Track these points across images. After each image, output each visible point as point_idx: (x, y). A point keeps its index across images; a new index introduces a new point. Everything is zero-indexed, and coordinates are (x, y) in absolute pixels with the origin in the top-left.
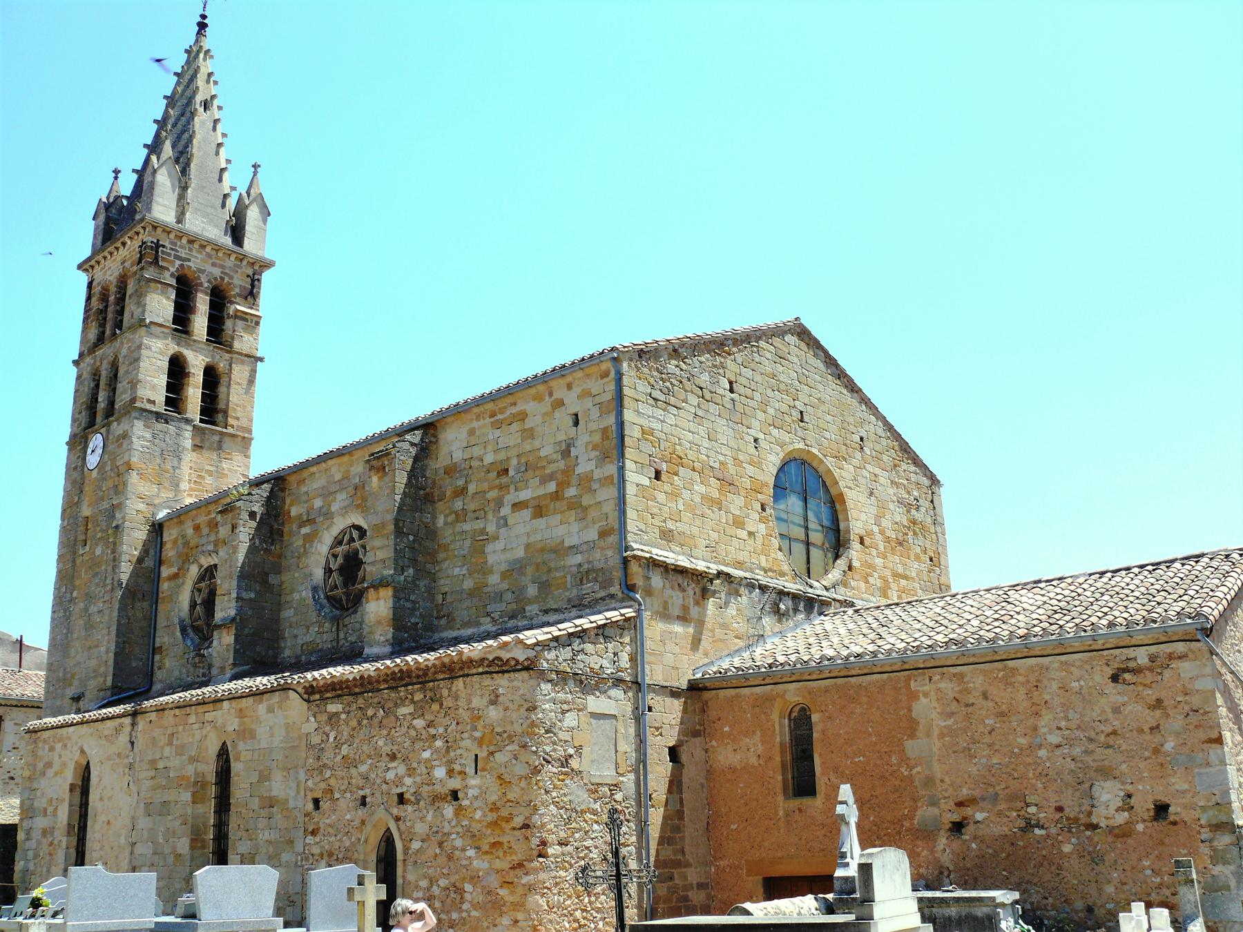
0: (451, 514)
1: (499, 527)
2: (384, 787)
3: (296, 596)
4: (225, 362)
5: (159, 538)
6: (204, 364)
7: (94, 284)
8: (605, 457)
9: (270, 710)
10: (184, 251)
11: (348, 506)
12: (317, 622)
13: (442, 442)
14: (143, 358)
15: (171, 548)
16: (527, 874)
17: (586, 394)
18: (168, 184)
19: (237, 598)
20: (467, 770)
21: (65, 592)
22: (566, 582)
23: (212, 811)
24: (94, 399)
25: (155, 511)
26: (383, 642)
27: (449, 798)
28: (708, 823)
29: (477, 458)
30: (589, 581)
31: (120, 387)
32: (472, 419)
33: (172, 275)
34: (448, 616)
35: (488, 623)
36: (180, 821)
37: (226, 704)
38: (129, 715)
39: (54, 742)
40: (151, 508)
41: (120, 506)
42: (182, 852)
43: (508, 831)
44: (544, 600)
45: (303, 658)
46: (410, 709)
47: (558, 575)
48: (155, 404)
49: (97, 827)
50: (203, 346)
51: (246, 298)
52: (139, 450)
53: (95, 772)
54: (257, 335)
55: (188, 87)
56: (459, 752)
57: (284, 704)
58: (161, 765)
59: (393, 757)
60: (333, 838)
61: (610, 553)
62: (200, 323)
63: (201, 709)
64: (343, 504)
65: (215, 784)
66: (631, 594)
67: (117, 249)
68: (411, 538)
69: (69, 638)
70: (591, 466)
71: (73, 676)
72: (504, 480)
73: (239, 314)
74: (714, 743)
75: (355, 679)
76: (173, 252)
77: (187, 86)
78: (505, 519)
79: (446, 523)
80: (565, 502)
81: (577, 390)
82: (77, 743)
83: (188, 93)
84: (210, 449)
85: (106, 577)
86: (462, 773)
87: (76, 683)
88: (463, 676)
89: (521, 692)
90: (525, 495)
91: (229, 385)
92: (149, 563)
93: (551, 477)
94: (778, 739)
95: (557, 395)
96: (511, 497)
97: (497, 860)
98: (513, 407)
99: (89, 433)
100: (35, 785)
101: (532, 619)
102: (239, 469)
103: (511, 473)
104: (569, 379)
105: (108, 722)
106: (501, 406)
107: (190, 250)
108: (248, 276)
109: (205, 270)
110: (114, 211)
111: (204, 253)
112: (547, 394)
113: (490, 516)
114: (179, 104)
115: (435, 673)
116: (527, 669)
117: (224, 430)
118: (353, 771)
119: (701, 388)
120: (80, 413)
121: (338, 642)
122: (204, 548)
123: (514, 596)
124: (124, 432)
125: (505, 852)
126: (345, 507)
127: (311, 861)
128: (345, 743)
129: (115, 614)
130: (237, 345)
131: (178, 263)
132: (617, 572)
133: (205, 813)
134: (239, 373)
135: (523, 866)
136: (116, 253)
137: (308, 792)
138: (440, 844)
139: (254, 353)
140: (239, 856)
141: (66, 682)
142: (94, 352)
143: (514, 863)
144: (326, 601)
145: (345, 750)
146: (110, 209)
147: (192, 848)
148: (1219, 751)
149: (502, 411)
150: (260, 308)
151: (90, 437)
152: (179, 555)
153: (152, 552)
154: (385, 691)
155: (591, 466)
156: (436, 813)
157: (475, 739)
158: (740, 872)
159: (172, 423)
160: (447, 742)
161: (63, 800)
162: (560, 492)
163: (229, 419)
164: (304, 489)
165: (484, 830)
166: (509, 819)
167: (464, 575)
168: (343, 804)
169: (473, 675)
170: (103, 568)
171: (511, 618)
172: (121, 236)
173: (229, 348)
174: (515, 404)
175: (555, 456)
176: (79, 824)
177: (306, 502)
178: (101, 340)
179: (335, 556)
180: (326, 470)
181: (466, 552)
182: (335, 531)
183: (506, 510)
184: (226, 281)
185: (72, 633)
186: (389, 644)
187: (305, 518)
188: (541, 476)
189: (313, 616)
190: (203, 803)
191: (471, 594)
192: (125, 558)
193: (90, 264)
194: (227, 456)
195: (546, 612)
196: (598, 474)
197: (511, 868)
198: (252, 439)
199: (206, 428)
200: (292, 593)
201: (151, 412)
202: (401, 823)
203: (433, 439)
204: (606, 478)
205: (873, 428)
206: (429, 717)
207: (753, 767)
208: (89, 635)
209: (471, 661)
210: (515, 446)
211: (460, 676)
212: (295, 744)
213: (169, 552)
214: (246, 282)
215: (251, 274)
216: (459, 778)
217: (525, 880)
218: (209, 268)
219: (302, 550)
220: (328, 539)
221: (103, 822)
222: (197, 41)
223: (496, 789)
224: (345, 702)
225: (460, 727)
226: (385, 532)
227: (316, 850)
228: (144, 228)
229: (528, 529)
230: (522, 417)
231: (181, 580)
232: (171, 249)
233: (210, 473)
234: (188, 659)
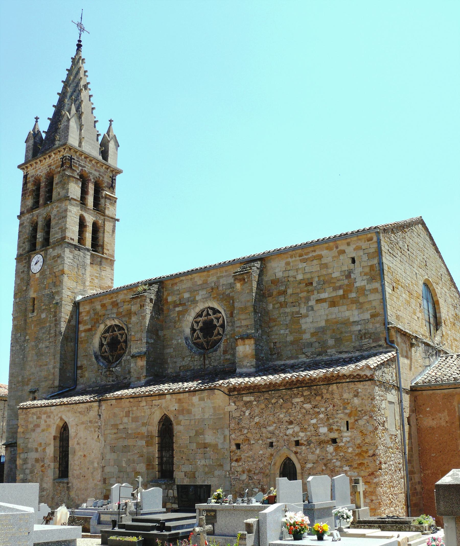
0: (277, 303)
1: (308, 310)
2: (285, 437)
3: (174, 342)
4: (102, 221)
5: (78, 310)
6: (93, 221)
7: (28, 176)
8: (372, 279)
9: (201, 399)
10: (83, 162)
11: (207, 297)
12: (189, 355)
13: (268, 268)
14: (68, 217)
15: (86, 316)
16: (375, 478)
17: (358, 248)
18: (75, 126)
19: (146, 342)
20: (342, 428)
21: (20, 336)
22: (352, 338)
23: (157, 451)
24: (34, 237)
25: (75, 296)
26: (249, 366)
27: (330, 442)
28: (419, 454)
29: (292, 276)
30: (365, 338)
31: (52, 231)
32: (288, 257)
33: (78, 174)
34: (278, 353)
35: (304, 358)
36: (138, 456)
37: (168, 397)
38: (97, 401)
39: (40, 414)
40: (74, 294)
41: (58, 293)
42: (140, 471)
43: (366, 458)
44: (339, 347)
45: (181, 374)
46: (302, 399)
47: (347, 335)
48: (74, 241)
49: (76, 458)
50: (91, 212)
51: (110, 188)
52: (67, 264)
53: (72, 430)
54: (116, 208)
55: (76, 77)
56: (336, 420)
57: (211, 397)
58: (121, 427)
59: (291, 423)
60: (251, 463)
61: (378, 325)
63: (149, 399)
64: (203, 296)
65: (158, 437)
66: (393, 345)
67: (45, 159)
68: (260, 315)
69: (25, 360)
70: (364, 283)
71: (29, 380)
72: (310, 288)
73: (108, 196)
74: (421, 416)
75: (266, 384)
76: (78, 163)
77: (75, 77)
78: (312, 307)
79: (274, 308)
80: (349, 300)
81: (353, 246)
82: (57, 415)
83: (76, 80)
84: (96, 264)
85: (50, 329)
86: (339, 430)
87: (31, 383)
88: (336, 383)
89: (369, 391)
90: (324, 295)
91: (104, 232)
92: (73, 323)
93: (340, 288)
94: (457, 414)
95: (341, 248)
96: (315, 296)
97: (362, 471)
98: (313, 252)
99: (32, 254)
100: (27, 436)
101: (331, 356)
102: (109, 276)
103: (315, 284)
104: (349, 240)
105: (81, 405)
106: (306, 251)
107: (85, 162)
108: (110, 177)
109: (92, 173)
110: (37, 139)
111: (91, 164)
112: (335, 247)
113: (302, 305)
114: (72, 85)
115: (319, 381)
116: (370, 380)
117: (103, 256)
118: (264, 430)
119: (401, 248)
120: (24, 243)
121: (205, 366)
122: (109, 316)
123: (319, 345)
124: (58, 254)
125: (366, 468)
126: (206, 298)
127: (236, 475)
128: (256, 416)
129: (59, 348)
130: (107, 212)
131: (80, 168)
132: (383, 334)
133: (153, 451)
134: (108, 226)
136: (44, 161)
137: (232, 441)
138: (325, 465)
139: (114, 217)
140: (184, 473)
141: (25, 382)
142: (32, 212)
143: (370, 472)
144: (193, 345)
145: (257, 419)
146: (36, 138)
147: (147, 469)
149: (307, 254)
150: (116, 194)
151: (32, 256)
152: (92, 319)
153: (74, 317)
154: (284, 390)
155: (364, 283)
156: (322, 450)
157: (346, 414)
158: (438, 476)
159: (81, 251)
160: (327, 415)
161: (50, 444)
162: (346, 295)
163: (105, 250)
164: (176, 288)
165: (354, 457)
166: (366, 452)
167: (287, 334)
168: (257, 447)
169: (344, 383)
170: (48, 324)
172: (50, 152)
173: (104, 214)
174: (315, 251)
175: (341, 277)
176: (59, 456)
177: (178, 294)
178: (36, 205)
180: (191, 279)
181: (287, 323)
182: (198, 310)
183: (312, 303)
184: (101, 179)
185: (27, 358)
186: (254, 367)
187: (178, 303)
188: (333, 287)
189: (187, 352)
190: (151, 446)
191: (292, 343)
192: (63, 320)
193: (26, 165)
194: (104, 269)
195: (341, 353)
196: (368, 287)
197: (368, 475)
198: (115, 261)
199: (95, 254)
200: (172, 340)
201: (72, 244)
202: (298, 455)
203: (264, 266)
204: (373, 289)
205: (443, 270)
206: (314, 403)
207: (444, 427)
208: (40, 359)
209: (345, 375)
210: (316, 272)
211: (334, 383)
212: (221, 417)
213: (84, 317)
214: (110, 180)
215: (112, 176)
217: (375, 480)
218: (93, 172)
219: (177, 319)
220: (193, 314)
221: (81, 455)
222: (77, 54)
223: (360, 437)
224: (256, 396)
225: (335, 408)
226: (247, 311)
227: (239, 469)
228: (64, 149)
229: (327, 312)
230: (320, 257)
231: (94, 332)
232: (77, 161)
234: (101, 373)
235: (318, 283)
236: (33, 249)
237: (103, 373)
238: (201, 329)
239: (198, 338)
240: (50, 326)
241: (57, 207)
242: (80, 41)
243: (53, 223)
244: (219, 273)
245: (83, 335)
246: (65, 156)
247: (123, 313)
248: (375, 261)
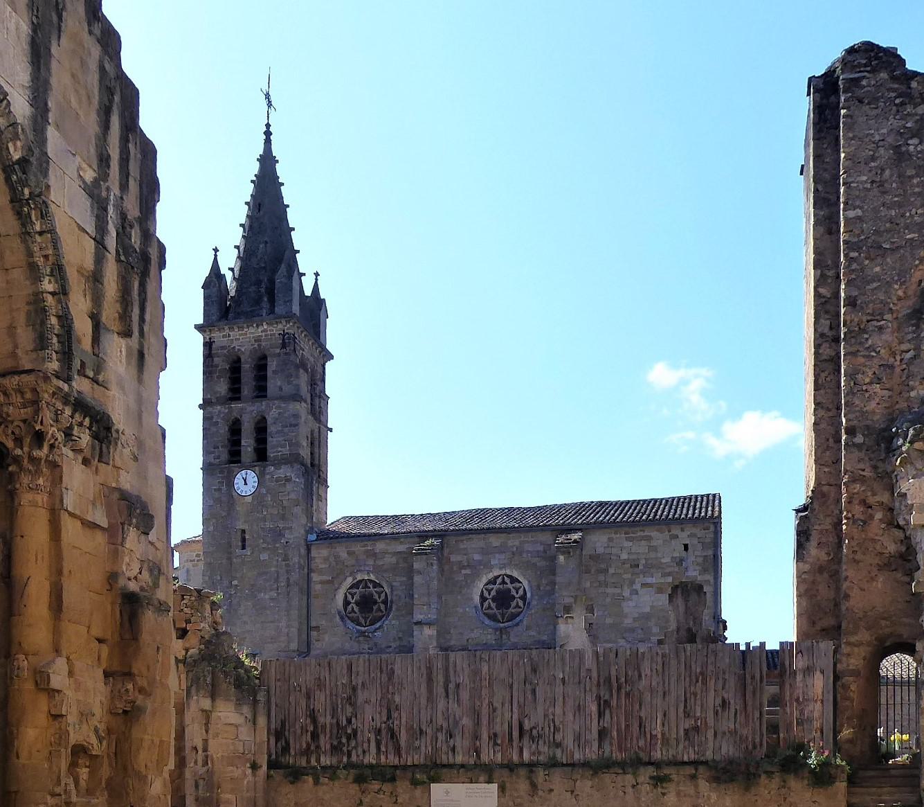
17: (691, 536)
72: (636, 570)
90: (649, 580)
93: (669, 574)
95: (674, 532)
103: (641, 567)
113: (626, 588)
121: (502, 641)
122: (362, 568)
148: (464, 759)
174: (644, 531)
175: (672, 564)
182: (491, 576)
183: (637, 586)
230: (649, 538)
235: (645, 566)
236: (235, 457)
237: (353, 638)
238: (494, 599)
239: (490, 607)
240: (278, 572)
241: (279, 407)
242: (268, 126)
243: (272, 429)
244: (523, 537)
245: (318, 587)
246: (287, 333)
247: (385, 567)
248: (710, 552)
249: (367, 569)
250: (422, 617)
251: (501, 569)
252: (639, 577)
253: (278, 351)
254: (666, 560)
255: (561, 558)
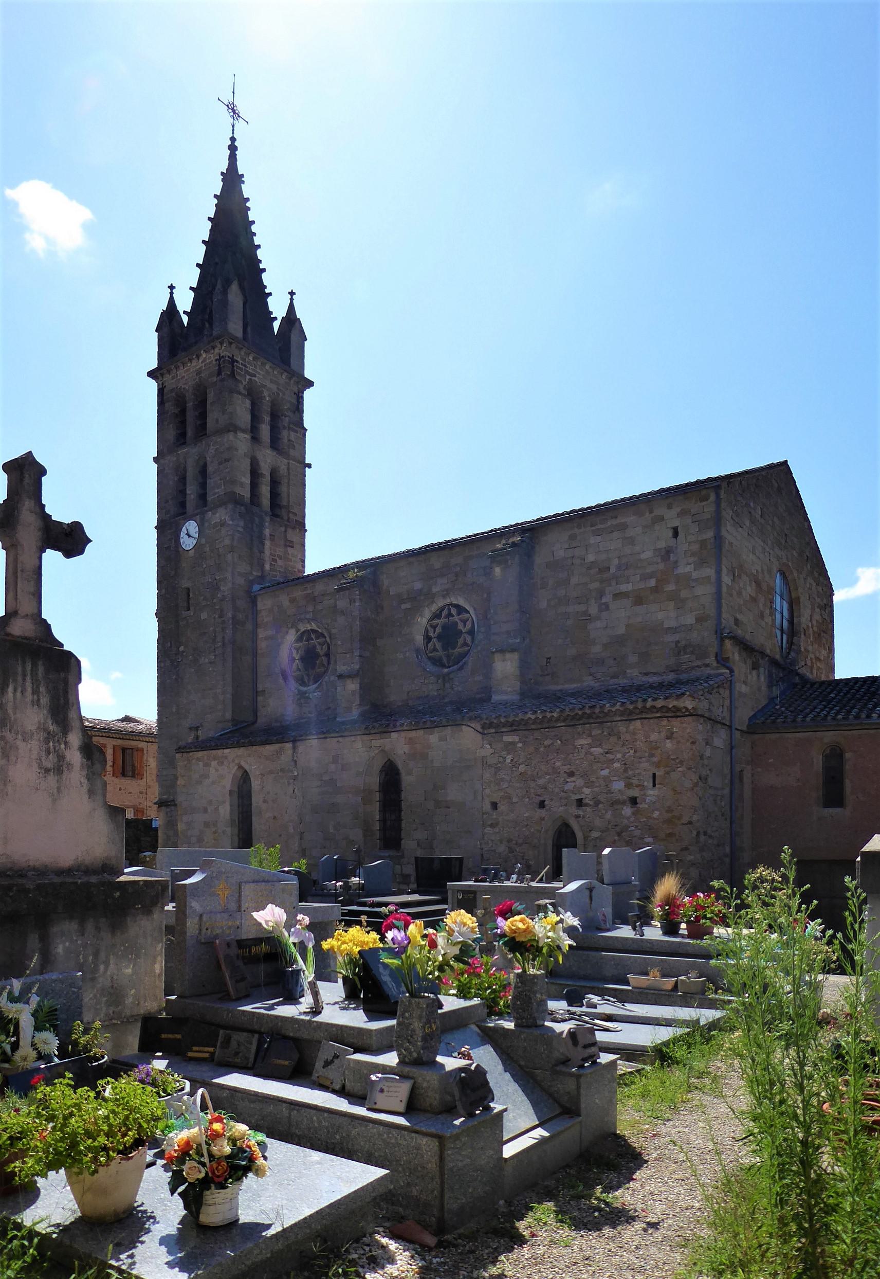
1: (601, 611)
30: (686, 653)
59: (571, 774)
62: (265, 431)
70: (688, 569)
82: (233, 761)
90: (624, 588)
103: (613, 570)
135: (688, 849)
145: (522, 768)
147: (365, 836)
166: (679, 818)
171: (612, 677)
179: (434, 627)
182: (434, 608)
183: (607, 599)
216: (637, 790)
233: (280, 558)
235: (619, 568)
242: (233, 139)
249: (308, 616)
250: (344, 668)
251: (444, 597)
252: (610, 586)
253: (215, 379)
254: (647, 555)
255: (497, 570)
